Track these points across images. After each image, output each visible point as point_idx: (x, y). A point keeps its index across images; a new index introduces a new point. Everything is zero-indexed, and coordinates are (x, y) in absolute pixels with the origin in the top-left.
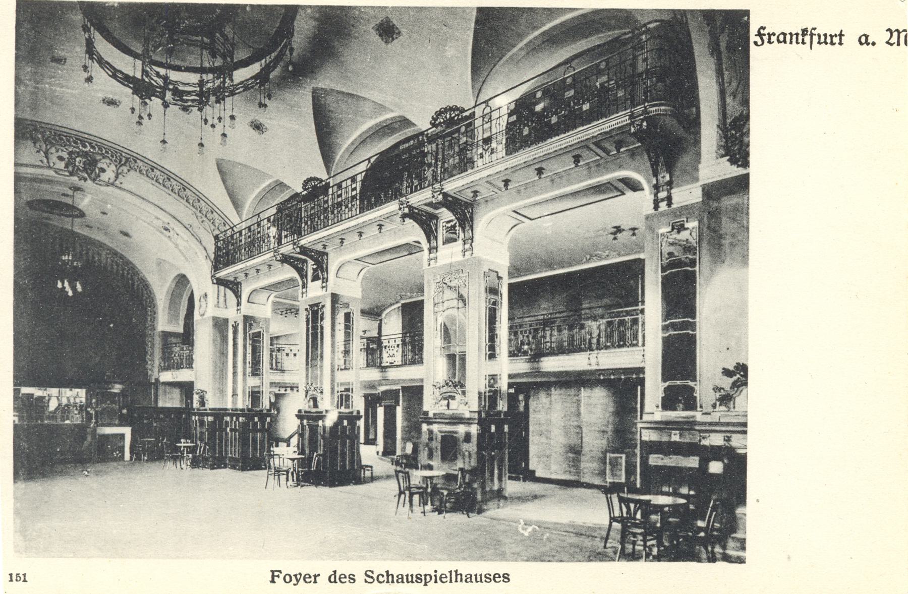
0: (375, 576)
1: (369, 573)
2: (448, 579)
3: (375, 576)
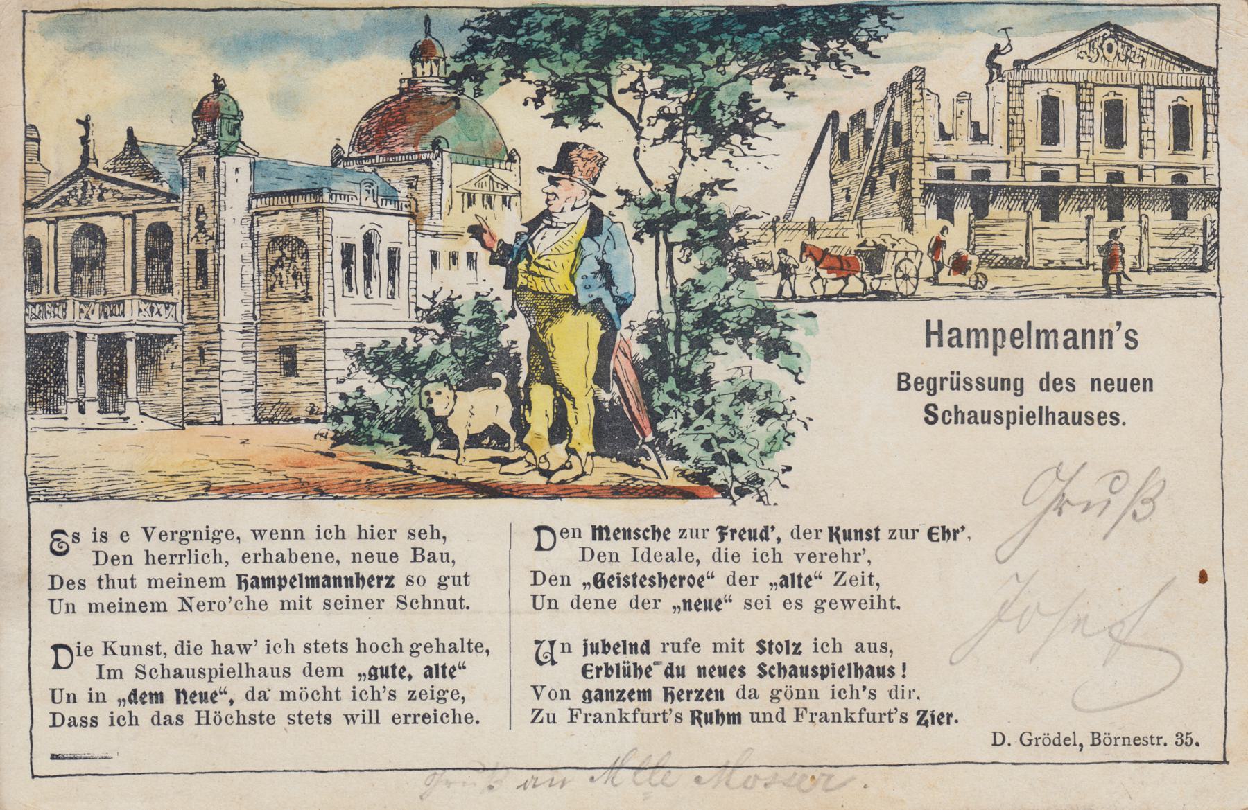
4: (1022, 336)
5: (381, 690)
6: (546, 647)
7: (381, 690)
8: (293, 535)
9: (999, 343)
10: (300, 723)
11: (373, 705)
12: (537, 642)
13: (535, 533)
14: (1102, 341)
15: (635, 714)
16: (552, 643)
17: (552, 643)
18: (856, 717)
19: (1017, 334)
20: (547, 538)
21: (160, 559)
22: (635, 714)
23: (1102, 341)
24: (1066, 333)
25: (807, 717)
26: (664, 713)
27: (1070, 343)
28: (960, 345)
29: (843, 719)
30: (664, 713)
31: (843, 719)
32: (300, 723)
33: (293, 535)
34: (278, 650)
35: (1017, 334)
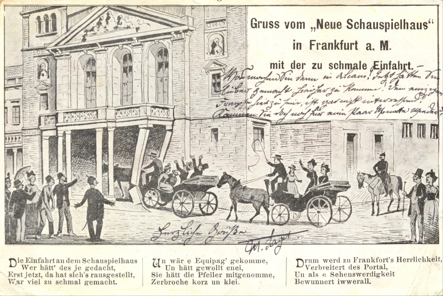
0: (353, 23)
1: (350, 21)
2: (118, 261)
3: (353, 23)
4: (398, 25)
5: (83, 273)
6: (156, 261)
7: (83, 273)
8: (315, 283)
9: (387, 27)
10: (120, 277)
11: (232, 265)
12: (154, 259)
13: (296, 261)
14: (301, 26)
15: (377, 259)
16: (159, 260)
17: (159, 260)
18: (375, 261)
19: (397, 24)
20: (300, 262)
21: (185, 282)
22: (377, 259)
23: (301, 26)
24: (354, 65)
25: (358, 260)
26: (387, 259)
27: (324, 48)
28: (414, 28)
29: (371, 261)
30: (387, 259)
31: (371, 261)
32: (120, 277)
33: (315, 283)
34: (77, 276)
35: (397, 24)
